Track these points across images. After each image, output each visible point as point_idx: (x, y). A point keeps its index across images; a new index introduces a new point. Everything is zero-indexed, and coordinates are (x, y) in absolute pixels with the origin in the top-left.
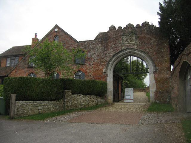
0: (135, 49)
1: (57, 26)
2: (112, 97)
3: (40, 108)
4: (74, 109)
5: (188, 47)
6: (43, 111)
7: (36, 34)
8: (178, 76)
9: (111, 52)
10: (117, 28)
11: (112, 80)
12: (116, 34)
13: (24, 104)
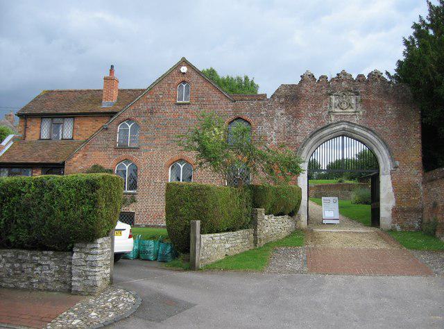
1: (184, 62)
3: (228, 246)
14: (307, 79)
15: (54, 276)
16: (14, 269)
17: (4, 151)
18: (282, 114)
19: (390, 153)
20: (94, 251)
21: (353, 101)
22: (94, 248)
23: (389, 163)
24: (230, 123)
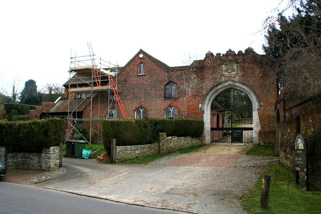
1: (141, 52)
2: (210, 137)
3: (137, 152)
4: (170, 152)
9: (208, 84)
10: (215, 55)
11: (209, 117)
14: (209, 55)
16: (23, 161)
18: (194, 78)
19: (258, 97)
20: (50, 152)
23: (256, 104)
24: (166, 85)
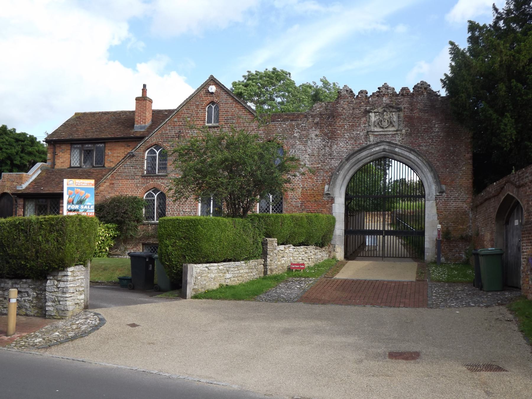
0: (396, 144)
5: (520, 173)
6: (234, 280)
7: (145, 86)
8: (494, 215)
10: (356, 93)
12: (353, 109)
13: (204, 269)
15: (32, 302)
17: (31, 180)
18: (316, 136)
21: (395, 118)
22: (65, 276)
23: (434, 187)
